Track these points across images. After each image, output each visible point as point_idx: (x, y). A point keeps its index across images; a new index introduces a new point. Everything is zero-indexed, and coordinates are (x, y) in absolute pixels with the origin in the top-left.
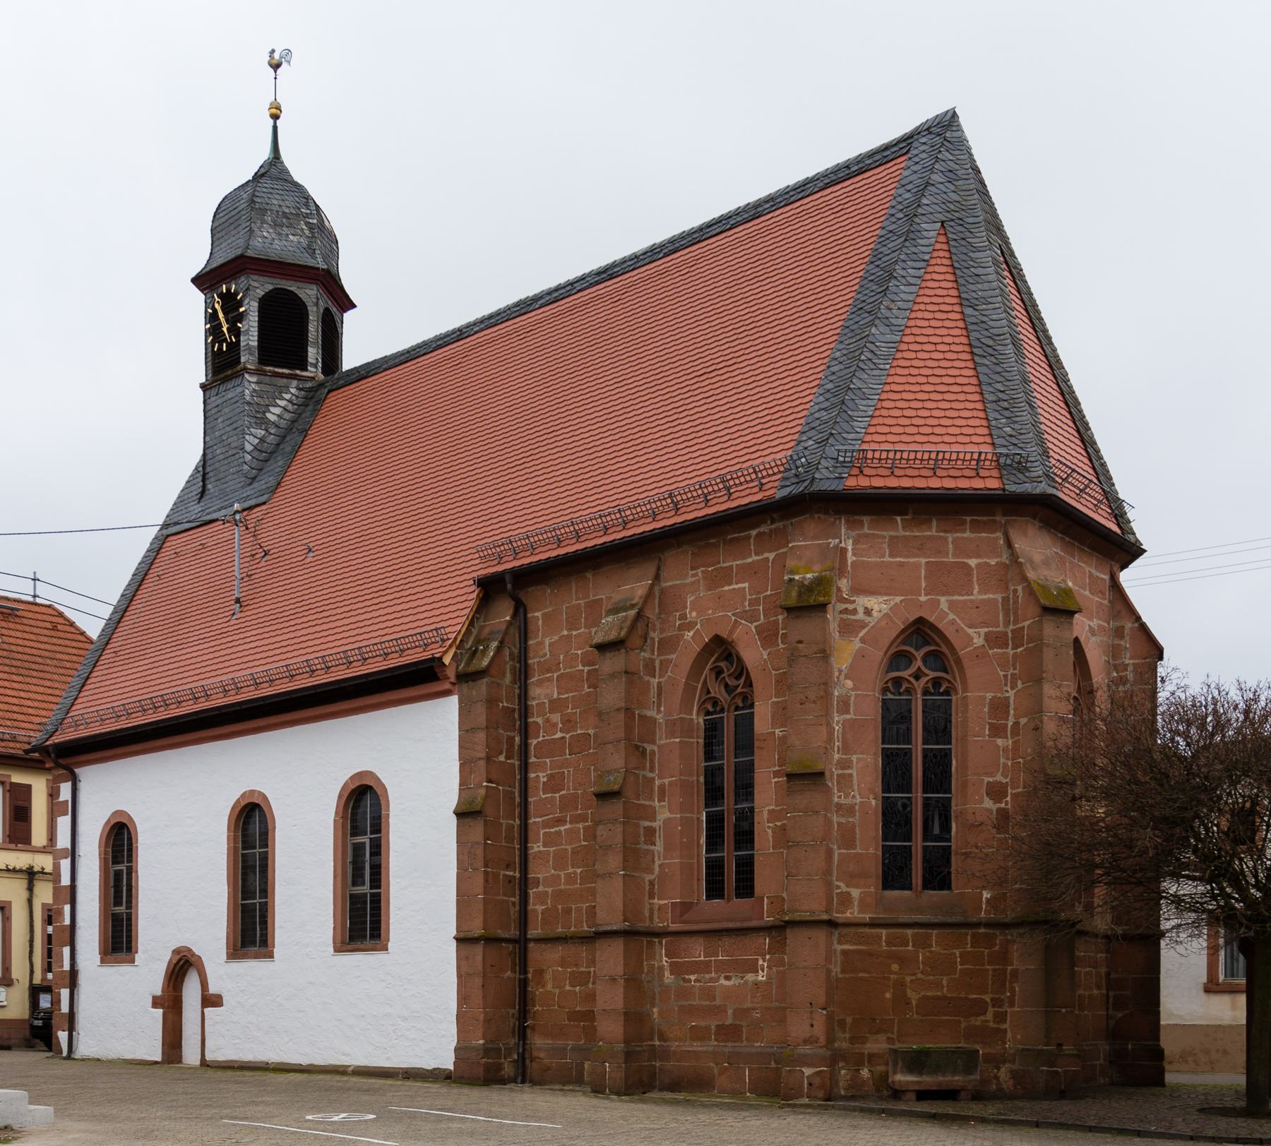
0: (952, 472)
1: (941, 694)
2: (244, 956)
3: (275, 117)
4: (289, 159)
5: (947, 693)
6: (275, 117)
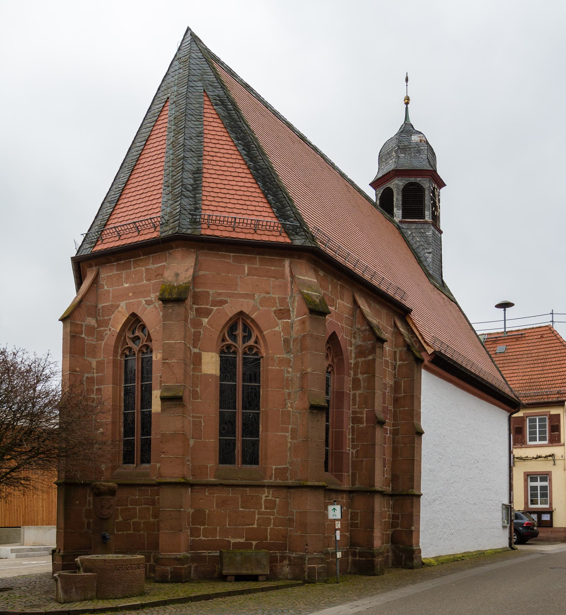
0: (244, 230)
1: (253, 355)
2: (503, 509)
3: (407, 104)
4: (412, 121)
5: (256, 354)
6: (407, 104)
